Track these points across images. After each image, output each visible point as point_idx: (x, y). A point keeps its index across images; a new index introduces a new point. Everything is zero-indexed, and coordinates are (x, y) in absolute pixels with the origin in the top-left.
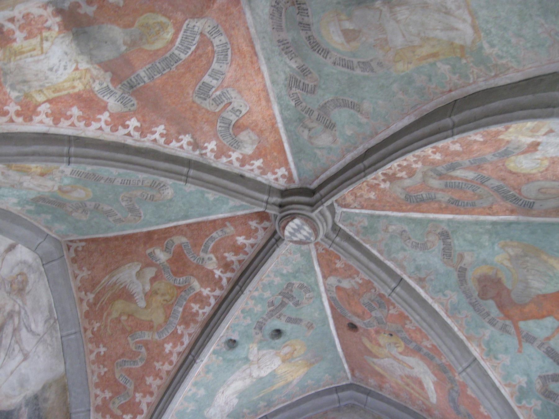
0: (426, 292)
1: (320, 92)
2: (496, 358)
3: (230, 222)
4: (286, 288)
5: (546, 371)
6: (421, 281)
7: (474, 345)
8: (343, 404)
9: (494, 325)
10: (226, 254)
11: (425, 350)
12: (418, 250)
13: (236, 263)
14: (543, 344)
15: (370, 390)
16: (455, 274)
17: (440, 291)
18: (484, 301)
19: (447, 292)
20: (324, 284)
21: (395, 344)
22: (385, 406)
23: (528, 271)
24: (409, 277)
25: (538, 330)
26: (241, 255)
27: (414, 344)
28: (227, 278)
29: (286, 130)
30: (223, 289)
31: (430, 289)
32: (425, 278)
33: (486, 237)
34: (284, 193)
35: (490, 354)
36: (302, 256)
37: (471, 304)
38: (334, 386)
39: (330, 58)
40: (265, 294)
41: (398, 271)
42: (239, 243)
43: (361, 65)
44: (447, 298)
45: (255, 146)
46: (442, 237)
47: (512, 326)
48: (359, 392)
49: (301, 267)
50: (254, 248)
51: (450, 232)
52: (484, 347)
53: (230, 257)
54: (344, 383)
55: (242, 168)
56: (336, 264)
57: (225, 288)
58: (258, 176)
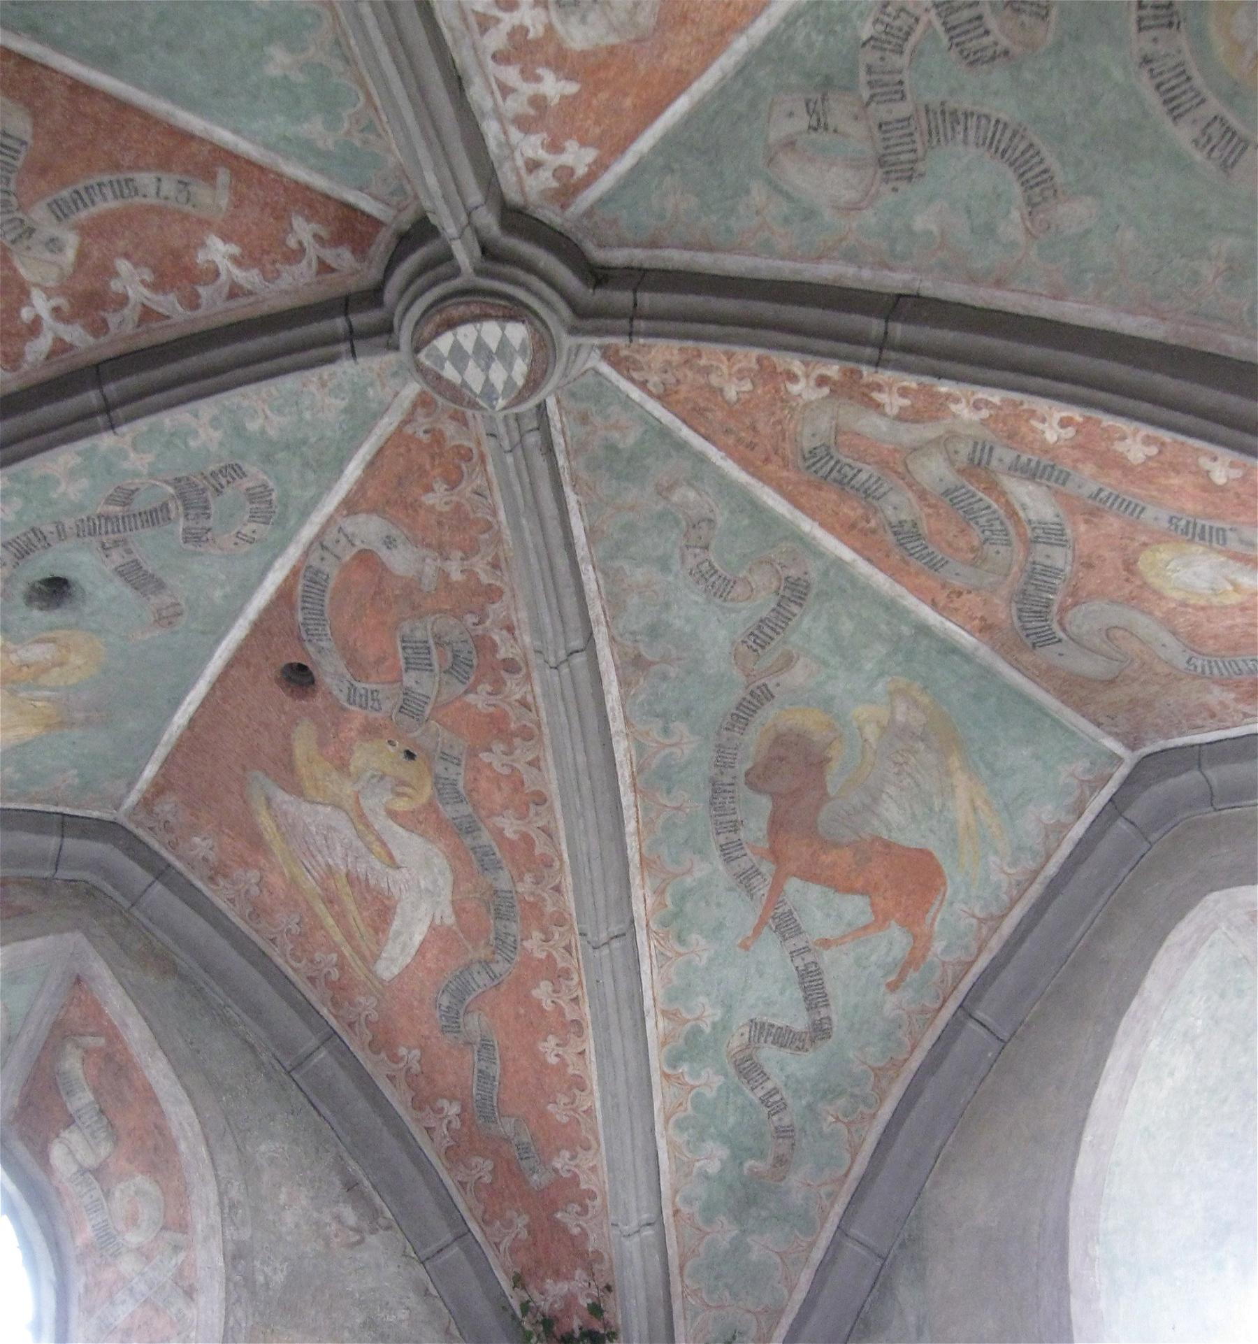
0: (624, 700)
1: (998, 77)
2: (681, 940)
3: (235, 174)
4: (213, 474)
5: (774, 1015)
6: (632, 665)
7: (648, 882)
8: (64, 874)
9: (728, 860)
10: (123, 266)
11: (486, 838)
12: (701, 587)
13: (130, 314)
14: (807, 949)
15: (169, 866)
16: (740, 693)
17: (664, 715)
18: (750, 794)
19: (680, 727)
20: (330, 520)
21: (403, 783)
22: (198, 927)
23: (898, 774)
24: (612, 639)
25: (819, 915)
26: (172, 297)
27: (466, 809)
28: (58, 340)
29: (743, 70)
30: (14, 369)
31: (642, 697)
32: (652, 663)
33: (881, 649)
34: (516, 218)
35: (674, 923)
36: (349, 410)
37: (713, 782)
38: (60, 809)
39: (1155, 40)
40: (132, 455)
41: (596, 610)
42: (201, 257)
43: (1216, 130)
44: (667, 741)
45: (613, 40)
46: (788, 593)
47: (770, 879)
48: (133, 858)
49: (313, 440)
50: (233, 304)
51: (814, 591)
52: (669, 901)
53: (131, 281)
54: (96, 814)
55: (490, 64)
56: (429, 489)
57: (26, 367)
58: (500, 118)
